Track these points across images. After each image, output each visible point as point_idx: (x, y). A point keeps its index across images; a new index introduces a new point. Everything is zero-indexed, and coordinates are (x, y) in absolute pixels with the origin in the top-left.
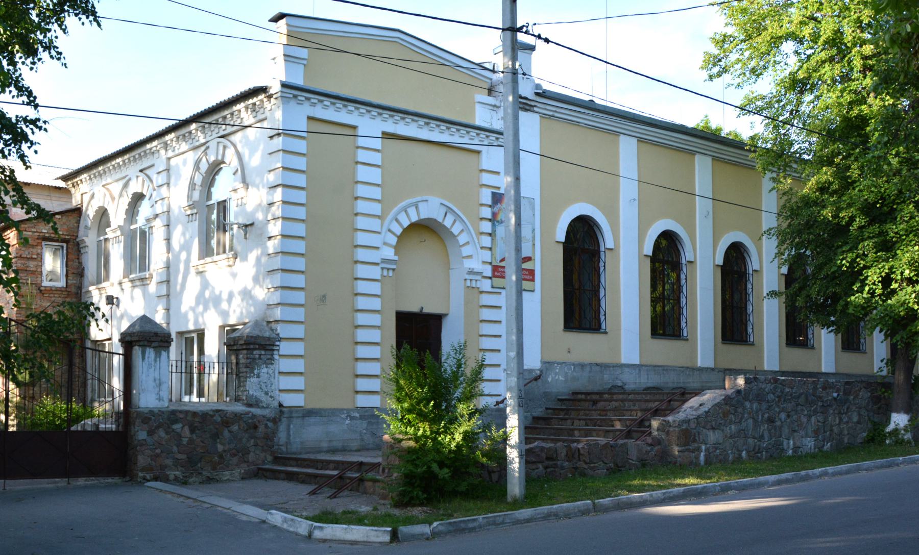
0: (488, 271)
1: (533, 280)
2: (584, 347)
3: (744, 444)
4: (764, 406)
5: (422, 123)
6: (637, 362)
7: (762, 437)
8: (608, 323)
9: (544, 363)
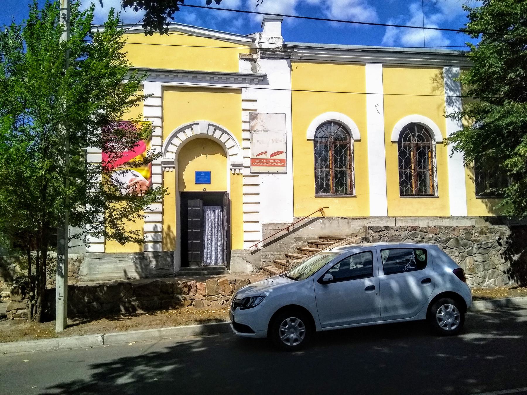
0: (247, 162)
2: (336, 206)
8: (356, 191)
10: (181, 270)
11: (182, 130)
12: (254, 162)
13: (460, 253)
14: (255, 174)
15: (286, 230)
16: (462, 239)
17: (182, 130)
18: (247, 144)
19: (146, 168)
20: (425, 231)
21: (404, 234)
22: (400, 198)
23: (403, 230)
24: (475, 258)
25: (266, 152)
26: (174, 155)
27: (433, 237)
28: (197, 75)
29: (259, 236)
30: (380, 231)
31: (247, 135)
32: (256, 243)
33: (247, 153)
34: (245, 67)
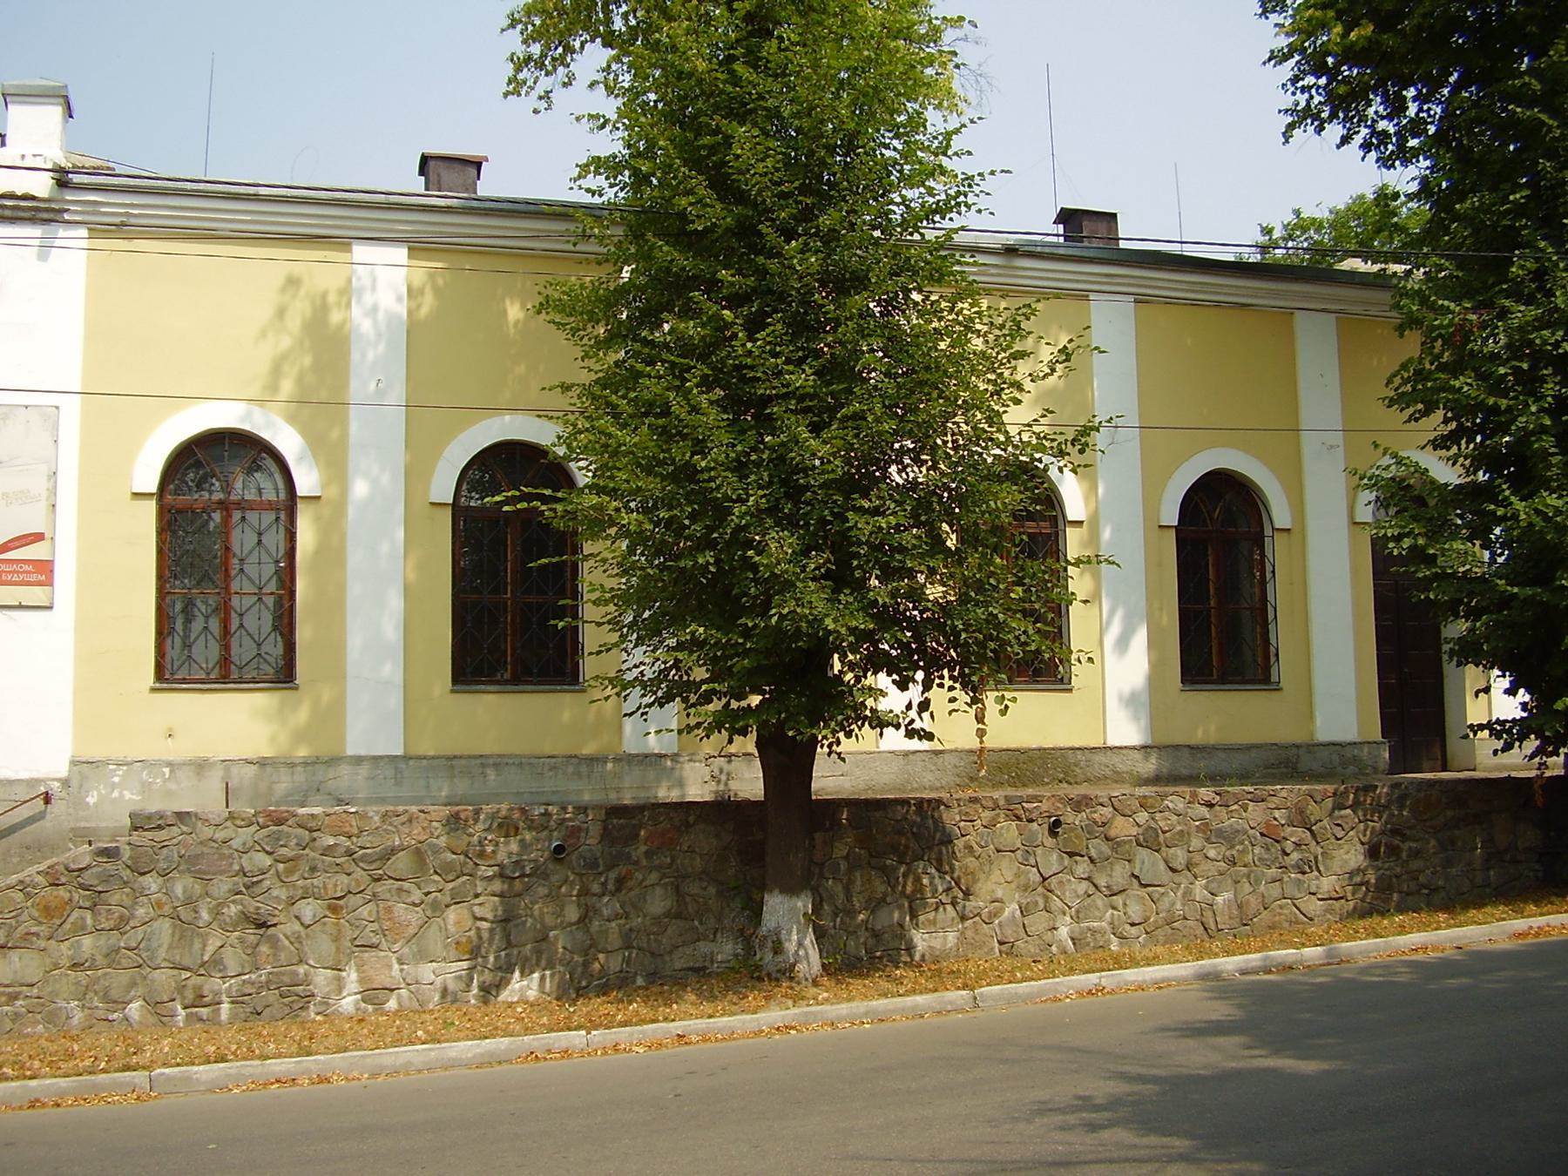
1: (49, 582)
3: (133, 984)
4: (222, 886)
6: (400, 752)
7: (216, 963)
8: (1286, 668)
9: (74, 763)
13: (427, 894)
16: (436, 850)
20: (312, 824)
21: (244, 835)
23: (239, 823)
24: (476, 909)
30: (160, 827)
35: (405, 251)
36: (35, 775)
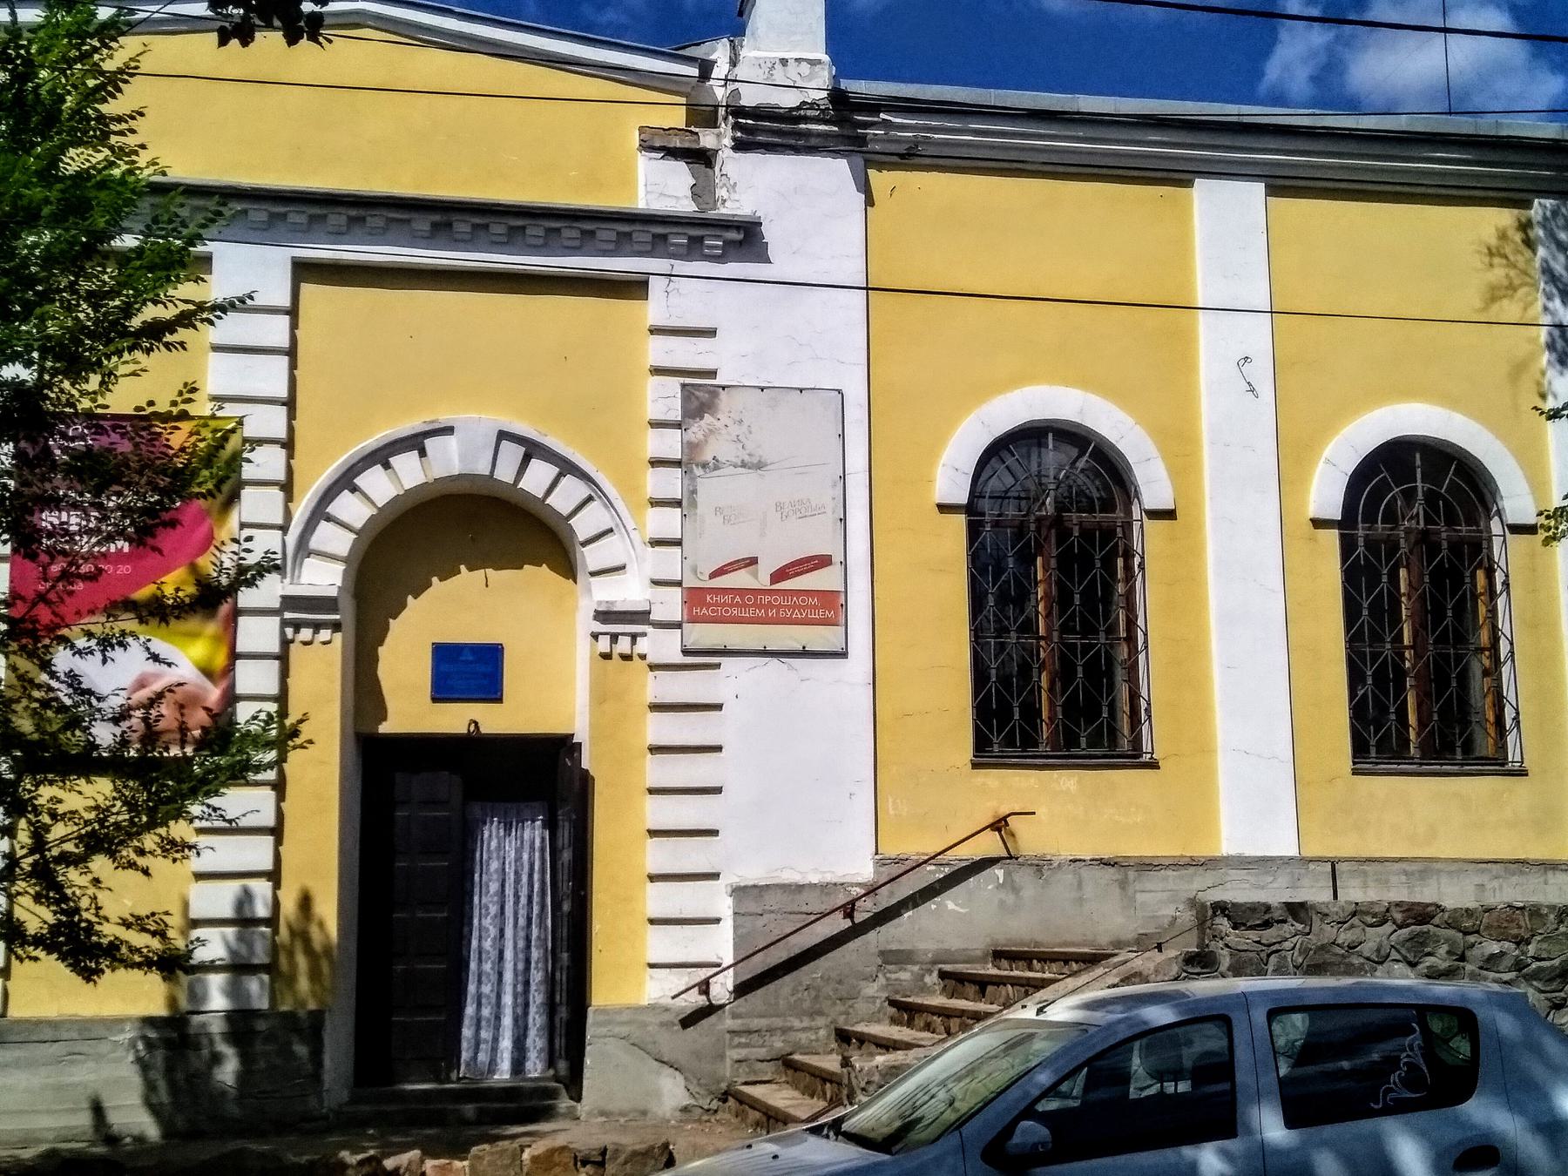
0: (670, 605)
2: (1064, 809)
5: (380, 222)
6: (1293, 852)
8: (1159, 737)
10: (354, 1101)
11: (381, 456)
12: (700, 603)
14: (702, 658)
15: (839, 915)
17: (381, 456)
18: (668, 522)
19: (212, 628)
20: (1468, 924)
21: (1374, 938)
22: (1355, 772)
23: (1369, 920)
25: (753, 561)
26: (340, 567)
27: (1502, 954)
28: (454, 217)
29: (720, 945)
30: (1267, 924)
31: (670, 483)
32: (703, 973)
33: (669, 563)
34: (662, 188)
35: (1259, 187)
36: (829, 878)
